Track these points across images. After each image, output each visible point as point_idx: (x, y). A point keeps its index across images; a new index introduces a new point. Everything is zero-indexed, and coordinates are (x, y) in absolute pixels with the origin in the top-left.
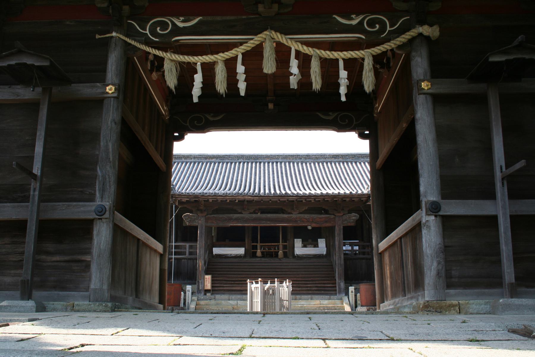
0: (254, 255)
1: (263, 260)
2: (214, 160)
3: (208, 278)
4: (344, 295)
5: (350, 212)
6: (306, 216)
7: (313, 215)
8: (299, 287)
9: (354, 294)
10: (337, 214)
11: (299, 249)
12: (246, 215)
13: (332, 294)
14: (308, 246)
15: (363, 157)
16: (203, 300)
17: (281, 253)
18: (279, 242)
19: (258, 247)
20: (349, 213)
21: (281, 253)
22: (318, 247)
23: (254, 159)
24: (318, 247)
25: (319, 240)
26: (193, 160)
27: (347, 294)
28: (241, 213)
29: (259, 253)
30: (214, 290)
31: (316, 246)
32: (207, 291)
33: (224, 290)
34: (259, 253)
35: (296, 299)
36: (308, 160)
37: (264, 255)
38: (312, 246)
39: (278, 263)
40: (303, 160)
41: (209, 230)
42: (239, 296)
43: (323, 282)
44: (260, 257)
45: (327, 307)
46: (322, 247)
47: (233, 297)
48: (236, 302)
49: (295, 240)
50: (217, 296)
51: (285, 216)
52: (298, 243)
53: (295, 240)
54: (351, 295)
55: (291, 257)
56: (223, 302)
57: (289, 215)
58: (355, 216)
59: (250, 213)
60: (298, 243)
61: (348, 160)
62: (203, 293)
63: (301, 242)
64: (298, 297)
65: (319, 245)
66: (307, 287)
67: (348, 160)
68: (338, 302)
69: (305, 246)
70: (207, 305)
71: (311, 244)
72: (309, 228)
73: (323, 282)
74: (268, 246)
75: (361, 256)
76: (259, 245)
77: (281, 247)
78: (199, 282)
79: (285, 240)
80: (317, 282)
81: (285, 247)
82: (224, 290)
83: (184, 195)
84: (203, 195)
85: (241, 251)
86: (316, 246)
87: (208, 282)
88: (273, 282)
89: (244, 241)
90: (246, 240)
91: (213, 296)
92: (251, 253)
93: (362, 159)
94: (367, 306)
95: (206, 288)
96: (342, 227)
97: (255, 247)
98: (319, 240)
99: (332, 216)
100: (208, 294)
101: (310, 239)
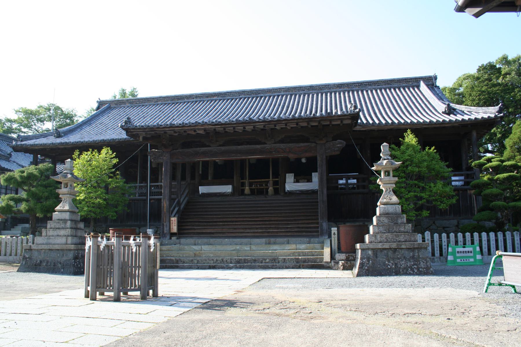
0: (242, 193)
1: (251, 198)
2: (215, 98)
3: (174, 220)
4: (327, 237)
5: (335, 139)
6: (282, 146)
7: (290, 144)
8: (278, 228)
9: (336, 236)
10: (318, 142)
11: (291, 185)
12: (214, 148)
13: (314, 236)
14: (300, 181)
15: (370, 85)
16: (167, 245)
17: (271, 189)
18: (269, 178)
19: (247, 184)
20: (333, 140)
21: (271, 189)
22: (311, 182)
23: (256, 94)
24: (311, 182)
25: (313, 174)
26: (195, 100)
27: (330, 236)
28: (209, 146)
29: (247, 190)
30: (181, 233)
31: (310, 180)
32: (172, 235)
33: (194, 233)
34: (247, 190)
35: (269, 243)
36: (311, 91)
37: (252, 192)
38: (306, 180)
39: (263, 200)
40: (306, 91)
41: (174, 166)
42: (205, 240)
43: (306, 222)
44: (248, 195)
45: (303, 252)
46: (315, 183)
47: (200, 241)
48: (200, 247)
49: (287, 175)
50: (183, 240)
51: (258, 147)
52: (290, 178)
53: (287, 175)
54: (335, 238)
55: (282, 194)
56: (186, 247)
57: (263, 146)
58: (340, 143)
59: (220, 146)
60: (290, 178)
61: (354, 89)
62: (168, 237)
63: (293, 177)
64: (272, 240)
65: (313, 180)
66: (288, 228)
67: (354, 89)
68: (318, 246)
69: (297, 181)
70: (169, 250)
71: (304, 179)
72: (304, 160)
73: (306, 222)
74: (260, 182)
75: (361, 190)
76: (247, 182)
77: (271, 182)
78: (163, 224)
79: (276, 175)
80: (300, 222)
81: (275, 183)
82: (194, 233)
83: (139, 129)
84: (159, 127)
85: (228, 189)
86: (310, 180)
87: (174, 225)
88: (128, 238)
89: (233, 178)
90: (235, 177)
91: (178, 241)
92: (238, 191)
93: (370, 87)
94: (346, 253)
95: (172, 231)
96: (325, 157)
97: (243, 184)
98: (313, 174)
99: (313, 145)
100: (174, 238)
101: (303, 173)
